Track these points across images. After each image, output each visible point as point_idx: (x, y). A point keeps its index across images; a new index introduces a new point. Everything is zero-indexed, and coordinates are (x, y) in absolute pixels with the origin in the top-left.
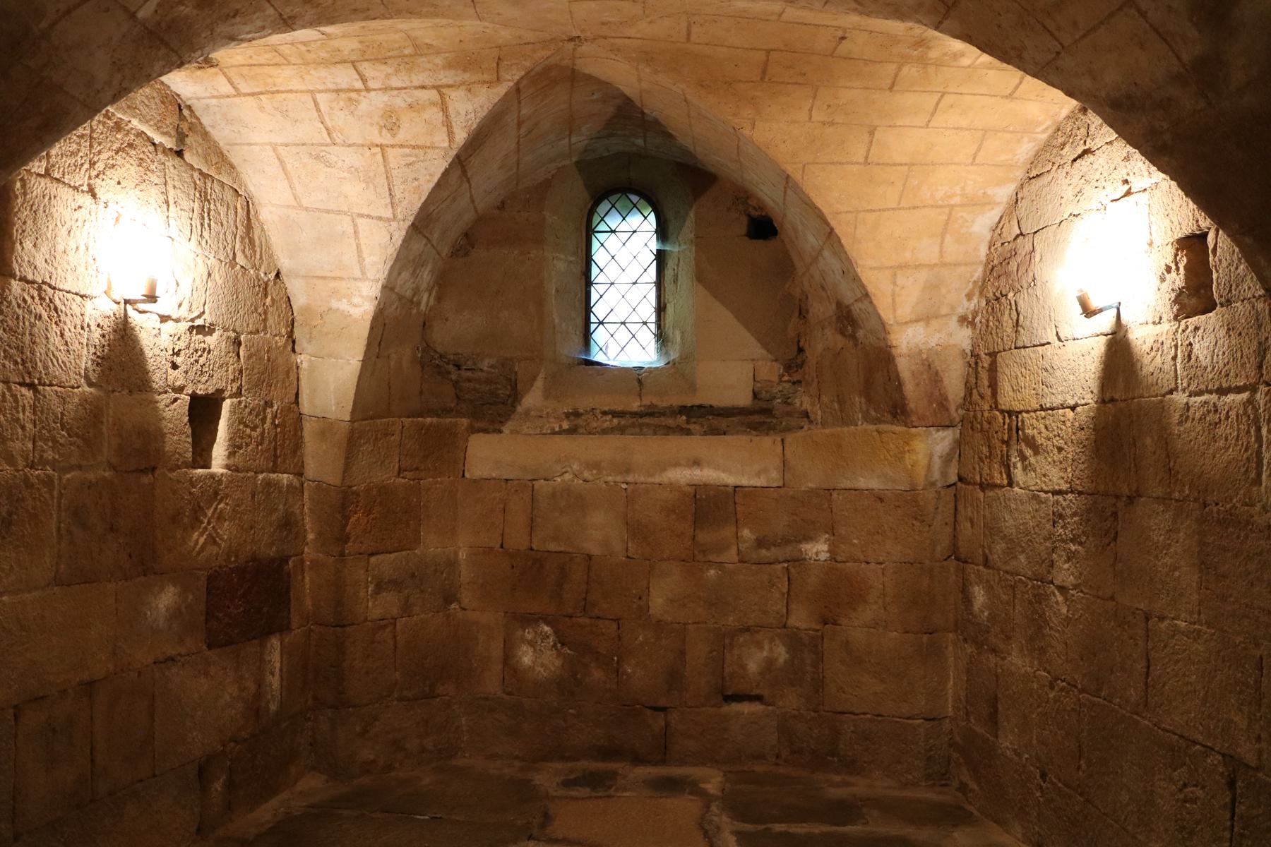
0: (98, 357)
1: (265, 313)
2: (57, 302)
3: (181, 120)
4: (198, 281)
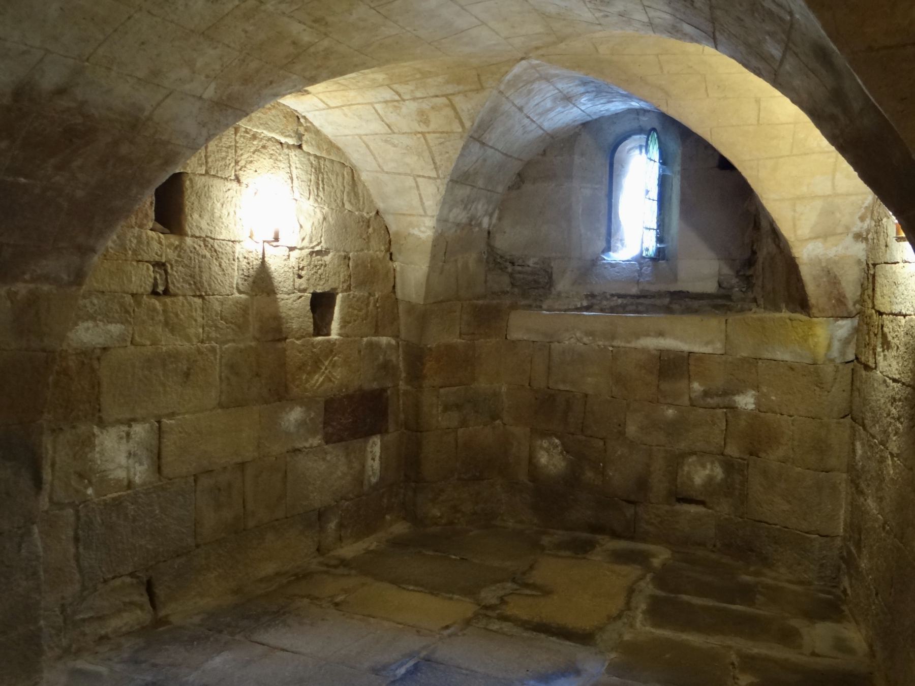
0: (245, 276)
1: (368, 237)
2: (216, 246)
3: (298, 125)
4: (316, 223)
